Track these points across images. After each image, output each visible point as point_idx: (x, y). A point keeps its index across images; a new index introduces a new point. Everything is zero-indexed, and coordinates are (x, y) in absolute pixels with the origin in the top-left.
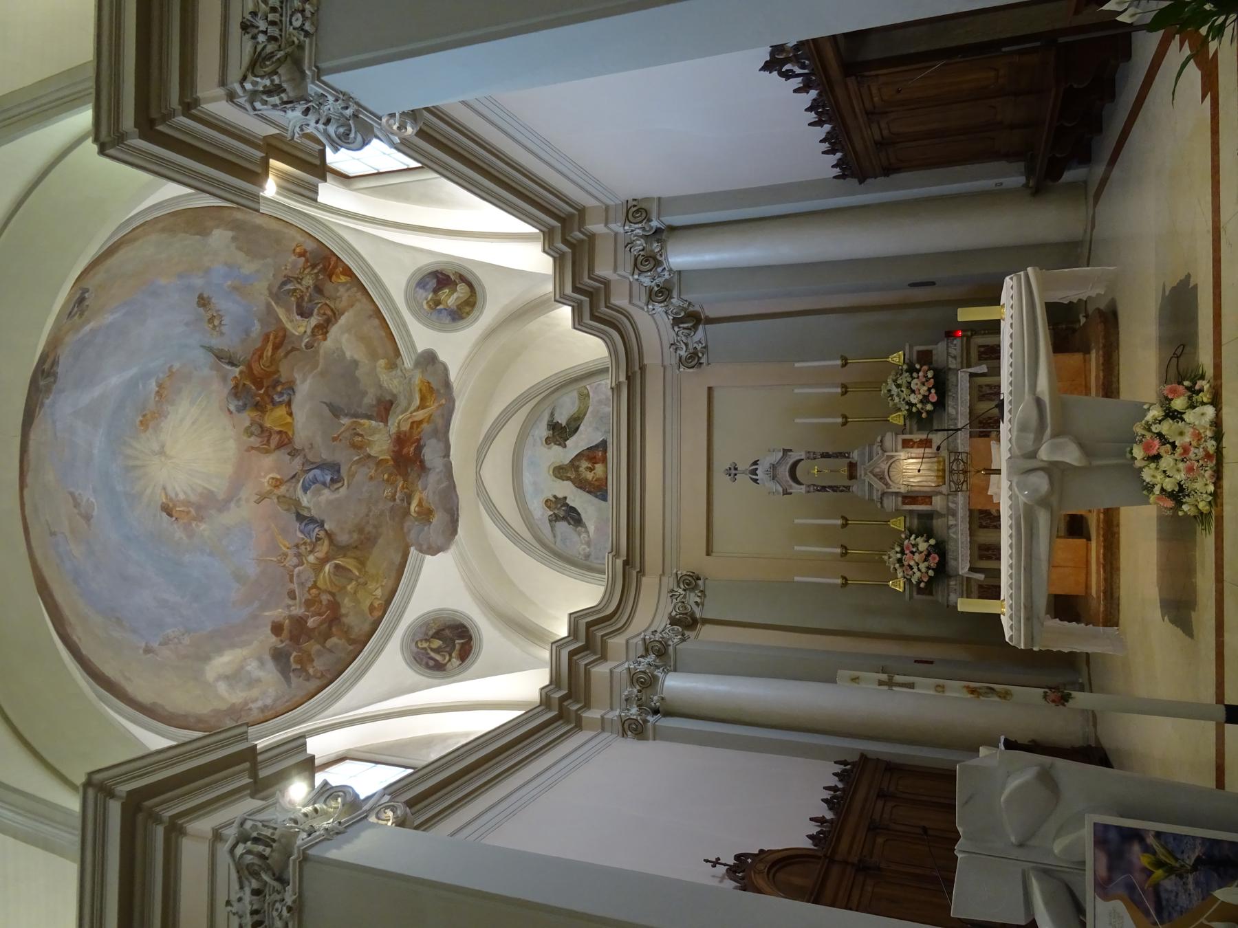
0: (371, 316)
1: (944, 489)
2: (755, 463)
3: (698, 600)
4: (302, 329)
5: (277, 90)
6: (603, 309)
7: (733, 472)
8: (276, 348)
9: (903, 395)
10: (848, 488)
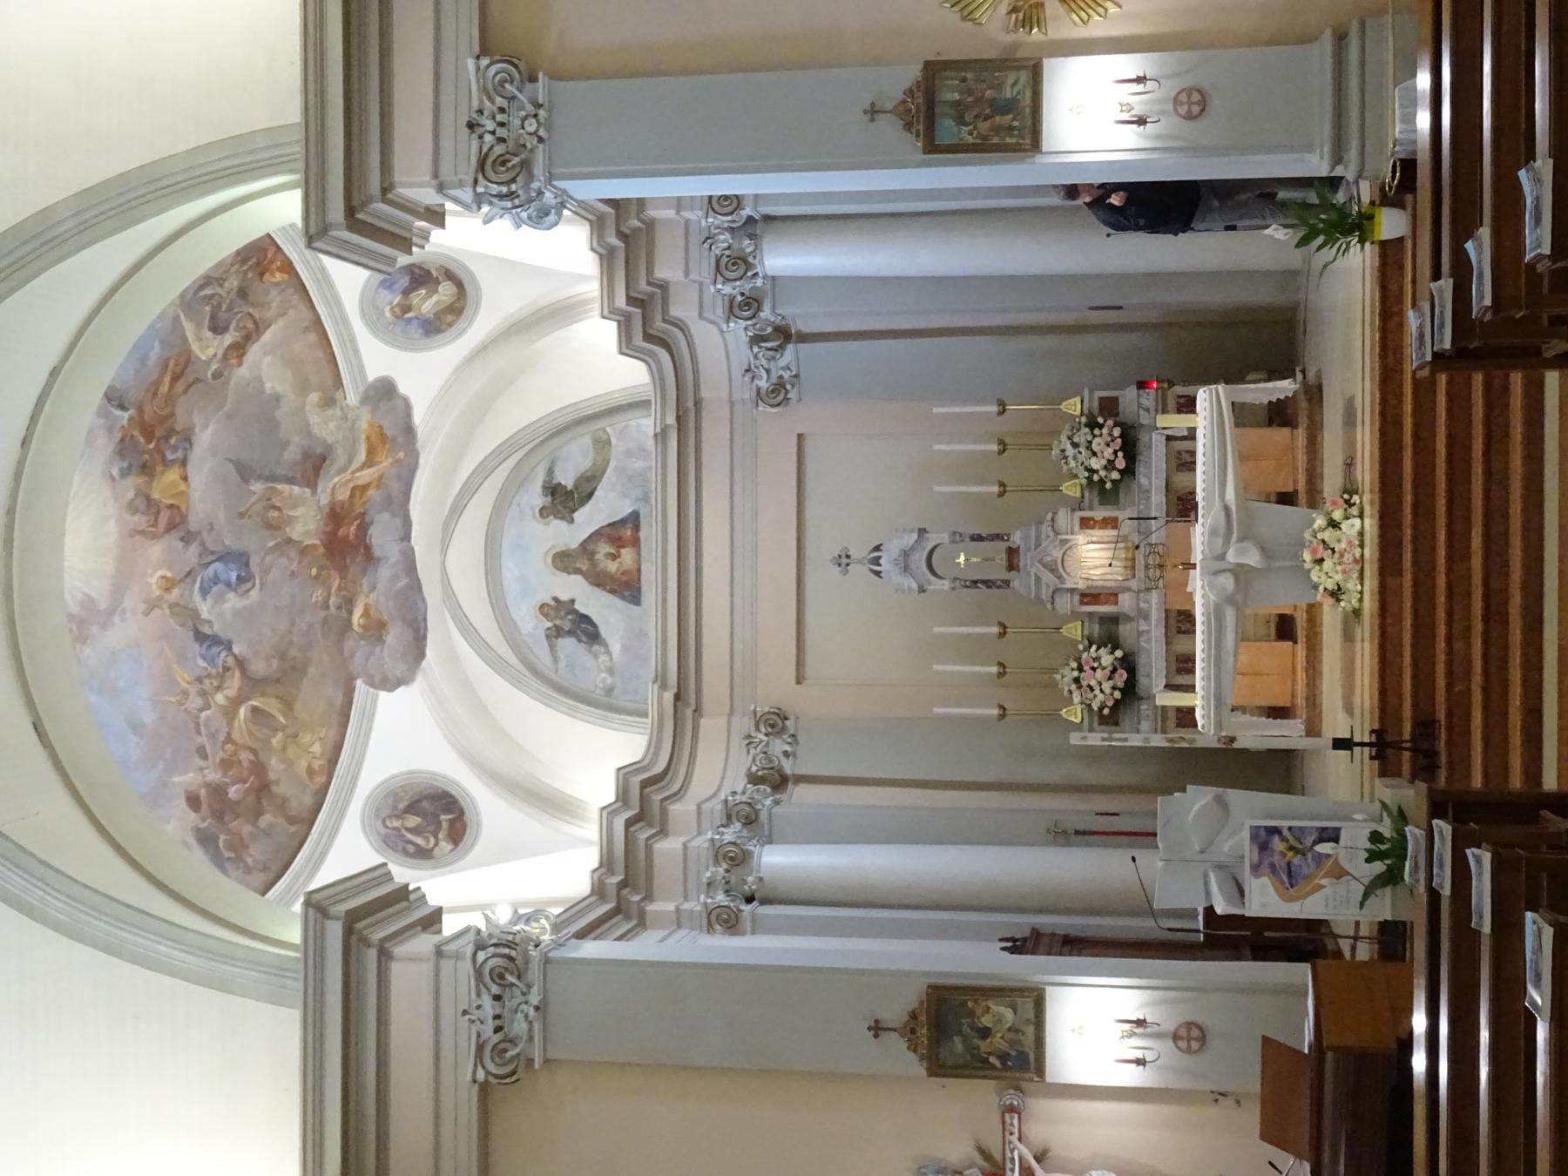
0: (307, 329)
1: (1133, 584)
2: (877, 548)
3: (788, 748)
4: (211, 352)
5: (511, 195)
6: (659, 324)
7: (843, 560)
8: (175, 379)
9: (1081, 458)
10: (1007, 583)
